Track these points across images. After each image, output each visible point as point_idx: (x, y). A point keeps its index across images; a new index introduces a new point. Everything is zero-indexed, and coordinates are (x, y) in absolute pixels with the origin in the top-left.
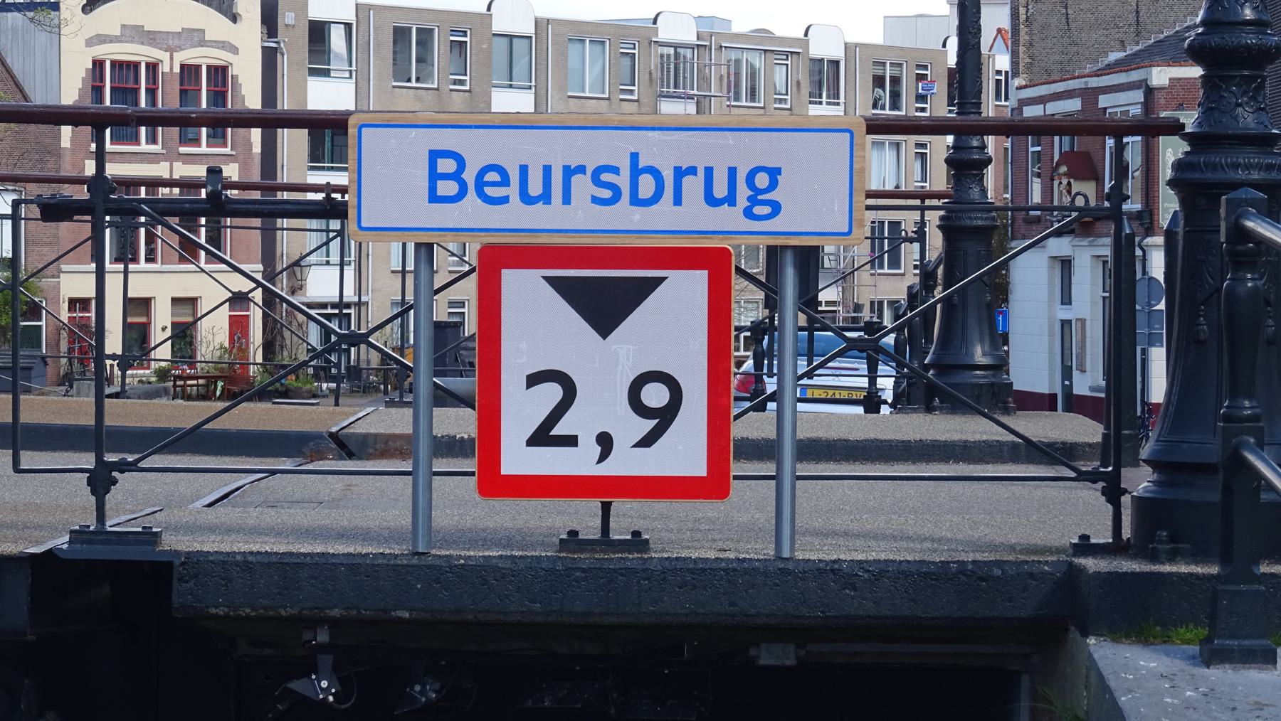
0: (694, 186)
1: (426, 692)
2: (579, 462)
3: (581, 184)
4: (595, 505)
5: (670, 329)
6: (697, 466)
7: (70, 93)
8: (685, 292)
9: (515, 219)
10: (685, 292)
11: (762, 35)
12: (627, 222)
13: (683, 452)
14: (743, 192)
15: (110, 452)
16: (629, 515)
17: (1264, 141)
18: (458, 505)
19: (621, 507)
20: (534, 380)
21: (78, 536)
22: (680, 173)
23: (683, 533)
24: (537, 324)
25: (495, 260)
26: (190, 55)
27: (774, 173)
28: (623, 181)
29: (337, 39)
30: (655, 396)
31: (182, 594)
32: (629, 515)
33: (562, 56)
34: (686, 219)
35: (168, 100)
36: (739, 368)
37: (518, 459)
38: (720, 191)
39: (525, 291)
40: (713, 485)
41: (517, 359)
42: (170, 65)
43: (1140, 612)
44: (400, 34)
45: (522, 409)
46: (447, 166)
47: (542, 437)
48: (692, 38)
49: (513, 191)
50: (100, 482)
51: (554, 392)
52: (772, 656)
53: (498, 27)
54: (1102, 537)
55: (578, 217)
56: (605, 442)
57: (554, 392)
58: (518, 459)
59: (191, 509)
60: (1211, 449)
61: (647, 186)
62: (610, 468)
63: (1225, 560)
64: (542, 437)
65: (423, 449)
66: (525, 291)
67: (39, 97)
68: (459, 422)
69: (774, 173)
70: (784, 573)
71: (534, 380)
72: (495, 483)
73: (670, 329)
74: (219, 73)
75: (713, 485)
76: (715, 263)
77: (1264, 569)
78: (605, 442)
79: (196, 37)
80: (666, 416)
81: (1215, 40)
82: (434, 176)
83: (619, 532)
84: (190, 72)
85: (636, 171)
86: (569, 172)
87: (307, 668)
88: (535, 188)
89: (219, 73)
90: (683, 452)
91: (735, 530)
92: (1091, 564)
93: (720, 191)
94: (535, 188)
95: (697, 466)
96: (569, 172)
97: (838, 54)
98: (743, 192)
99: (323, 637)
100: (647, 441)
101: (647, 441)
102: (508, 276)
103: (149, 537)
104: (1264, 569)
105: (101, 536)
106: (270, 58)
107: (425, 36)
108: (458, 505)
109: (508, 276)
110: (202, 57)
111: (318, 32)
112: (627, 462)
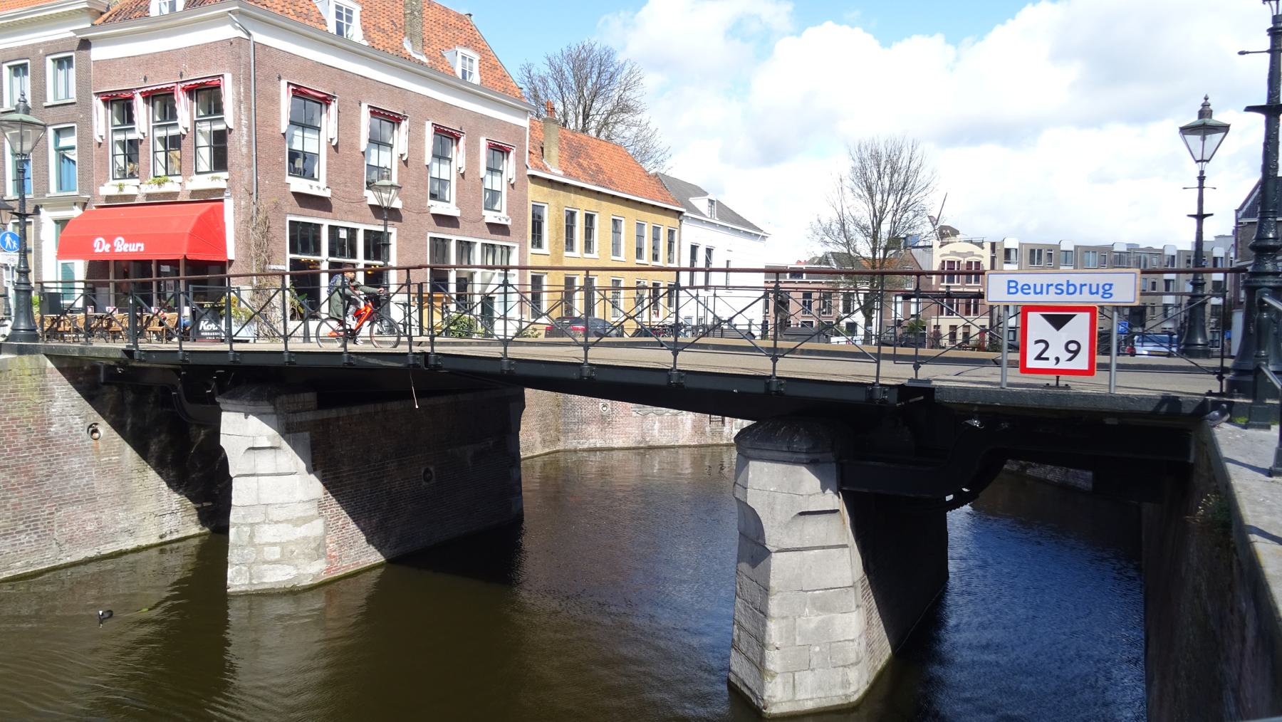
0: (1085, 289)
1: (1005, 425)
2: (1050, 365)
3: (1085, 289)
4: (1054, 377)
5: (1079, 327)
6: (1086, 367)
7: (936, 267)
8: (1082, 320)
9: (1032, 298)
10: (1082, 320)
11: (1150, 248)
12: (1065, 299)
13: (1082, 362)
14: (1101, 291)
15: (676, 348)
16: (1064, 379)
17: (1276, 274)
18: (1014, 376)
19: (1062, 377)
20: (1037, 342)
21: (911, 380)
22: (1082, 286)
23: (1083, 386)
24: (1038, 326)
25: (1026, 310)
26: (969, 259)
27: (1111, 285)
28: (1064, 288)
29: (1013, 253)
30: (1073, 347)
31: (938, 396)
32: (1064, 379)
33: (1082, 257)
34: (1084, 298)
35: (963, 268)
36: (1101, 342)
37: (1031, 363)
38: (1094, 290)
39: (1035, 319)
40: (1090, 372)
41: (1032, 336)
42: (964, 261)
43: (1231, 412)
44: (1032, 251)
45: (1033, 350)
46: (1013, 284)
47: (1039, 358)
48: (1125, 249)
49: (1032, 291)
50: (916, 368)
51: (1043, 346)
52: (1109, 421)
53: (1062, 248)
54: (1217, 390)
55: (1051, 298)
56: (1057, 359)
57: (1043, 346)
58: (1031, 363)
59: (941, 376)
60: (1250, 365)
61: (1071, 289)
62: (1059, 367)
63: (1254, 398)
64: (1039, 358)
65: (1005, 362)
66: (1035, 319)
67: (925, 268)
68: (1016, 356)
69: (1111, 285)
70: (1112, 398)
71: (1037, 342)
72: (1025, 370)
73: (1079, 327)
74: (978, 263)
75: (1090, 372)
76: (1091, 310)
77: (1268, 401)
78: (1057, 359)
79: (971, 254)
80: (1076, 353)
81: (1258, 244)
82: (1009, 287)
83: (1062, 383)
84: (969, 263)
85: (1068, 285)
86: (1048, 286)
87: (972, 418)
88: (1038, 290)
89: (978, 263)
90: (1082, 362)
91: (1097, 385)
92: (1050, 391)
93: (1094, 290)
94: (1038, 290)
95: (1086, 367)
96: (1048, 286)
97: (1175, 253)
98: (1101, 291)
99: (976, 409)
100: (1070, 359)
101: (1070, 359)
102: (1030, 314)
103: (929, 381)
104: (1268, 401)
105: (916, 380)
106: (993, 259)
107: (1040, 251)
108: (1014, 376)
109: (1030, 314)
110: (973, 259)
111: (1008, 251)
112: (1063, 365)
